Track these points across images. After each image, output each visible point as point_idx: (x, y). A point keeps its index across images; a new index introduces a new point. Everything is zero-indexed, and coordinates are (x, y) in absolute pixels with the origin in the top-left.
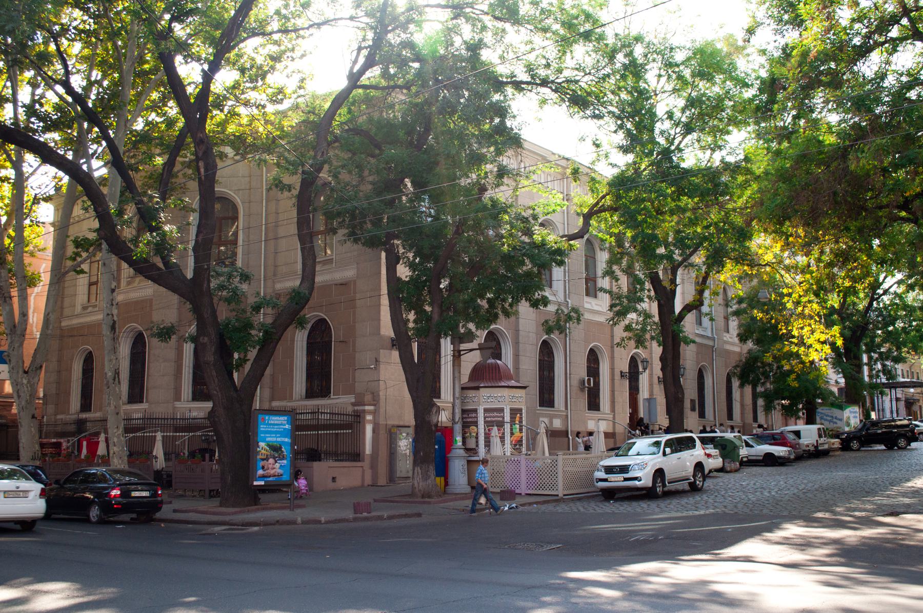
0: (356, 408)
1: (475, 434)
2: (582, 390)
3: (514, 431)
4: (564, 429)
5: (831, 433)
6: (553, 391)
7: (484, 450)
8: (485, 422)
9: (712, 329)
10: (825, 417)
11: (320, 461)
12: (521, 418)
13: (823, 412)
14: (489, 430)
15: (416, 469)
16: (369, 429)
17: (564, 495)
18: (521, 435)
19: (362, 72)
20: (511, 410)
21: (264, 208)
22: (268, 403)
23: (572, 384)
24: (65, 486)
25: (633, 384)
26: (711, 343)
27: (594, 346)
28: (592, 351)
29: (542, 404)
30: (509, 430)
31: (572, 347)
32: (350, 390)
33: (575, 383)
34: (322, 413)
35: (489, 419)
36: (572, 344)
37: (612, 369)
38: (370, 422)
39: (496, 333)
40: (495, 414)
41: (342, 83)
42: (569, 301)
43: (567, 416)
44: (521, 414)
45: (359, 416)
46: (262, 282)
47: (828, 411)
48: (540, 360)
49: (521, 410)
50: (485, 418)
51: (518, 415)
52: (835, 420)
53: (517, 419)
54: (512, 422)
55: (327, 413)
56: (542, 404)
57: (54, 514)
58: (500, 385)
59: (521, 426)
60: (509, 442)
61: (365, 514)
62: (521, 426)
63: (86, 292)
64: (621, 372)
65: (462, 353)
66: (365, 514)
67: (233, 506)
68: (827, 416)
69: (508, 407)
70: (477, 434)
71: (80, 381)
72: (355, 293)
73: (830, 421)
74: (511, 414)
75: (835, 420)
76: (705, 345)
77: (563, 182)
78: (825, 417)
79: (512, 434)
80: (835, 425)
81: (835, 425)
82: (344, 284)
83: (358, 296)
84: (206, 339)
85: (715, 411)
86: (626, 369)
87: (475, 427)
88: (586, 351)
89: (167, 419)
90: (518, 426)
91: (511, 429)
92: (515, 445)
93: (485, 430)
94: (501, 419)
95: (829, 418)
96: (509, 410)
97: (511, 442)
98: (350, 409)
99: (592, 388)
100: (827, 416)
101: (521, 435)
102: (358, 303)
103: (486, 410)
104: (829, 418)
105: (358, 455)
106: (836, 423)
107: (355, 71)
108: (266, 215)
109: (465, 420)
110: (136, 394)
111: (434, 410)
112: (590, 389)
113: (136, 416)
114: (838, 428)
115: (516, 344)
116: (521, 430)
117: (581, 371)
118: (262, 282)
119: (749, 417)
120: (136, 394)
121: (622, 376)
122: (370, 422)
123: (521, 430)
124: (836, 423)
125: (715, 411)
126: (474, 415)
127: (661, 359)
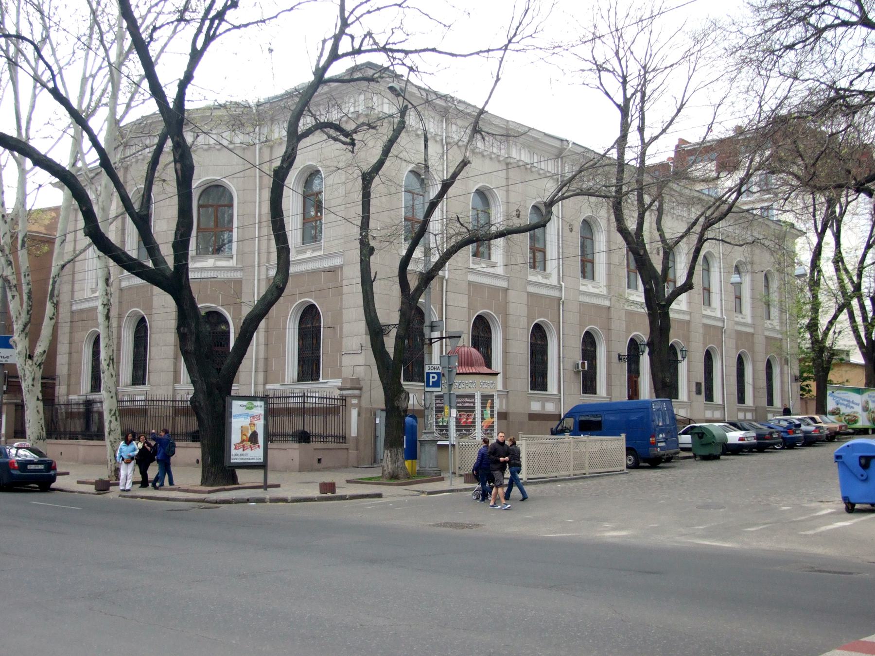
0: (342, 392)
2: (577, 372)
3: (485, 416)
4: (557, 413)
5: (847, 418)
6: (547, 374)
7: (455, 435)
9: (722, 309)
10: (841, 401)
11: (309, 442)
12: (492, 404)
13: (839, 396)
14: (460, 415)
15: (386, 451)
16: (354, 413)
17: (528, 479)
18: (492, 420)
19: (325, 68)
20: (482, 396)
21: (257, 196)
22: (262, 386)
24: (869, 321)
25: (633, 366)
26: (720, 324)
27: (591, 329)
28: (588, 334)
29: (533, 388)
30: (480, 416)
32: (337, 374)
33: (570, 366)
34: (307, 397)
35: (460, 405)
37: (609, 352)
38: (354, 406)
39: (486, 317)
41: (311, 78)
42: (563, 284)
43: (560, 399)
44: (493, 400)
45: (345, 400)
46: (256, 268)
47: (844, 395)
48: (531, 344)
49: (492, 396)
50: (436, 404)
51: (490, 401)
52: (851, 405)
53: (489, 405)
54: (484, 407)
55: (316, 397)
56: (533, 388)
59: (492, 411)
61: (329, 494)
62: (492, 411)
63: (358, 196)
64: (619, 355)
65: (433, 341)
66: (329, 494)
67: (212, 486)
68: (844, 400)
71: (90, 365)
72: (342, 280)
73: (847, 406)
74: (482, 400)
75: (851, 405)
76: (714, 327)
77: (558, 162)
78: (841, 401)
79: (483, 419)
80: (852, 410)
81: (852, 410)
82: (332, 270)
83: (345, 283)
84: (186, 329)
85: (723, 394)
86: (625, 352)
88: (581, 335)
89: (167, 401)
91: (482, 415)
92: (486, 430)
94: (472, 405)
95: (846, 403)
97: (482, 427)
98: (336, 393)
99: (586, 371)
100: (844, 400)
101: (492, 420)
102: (345, 289)
104: (846, 403)
105: (344, 437)
106: (853, 408)
107: (320, 66)
108: (259, 202)
109: (437, 405)
110: (139, 376)
111: (403, 396)
112: (584, 373)
113: (138, 398)
114: (854, 413)
115: (505, 328)
117: (576, 355)
118: (256, 268)
119: (764, 401)
120: (139, 376)
121: (620, 359)
122: (354, 406)
123: (492, 416)
124: (853, 408)
125: (723, 394)
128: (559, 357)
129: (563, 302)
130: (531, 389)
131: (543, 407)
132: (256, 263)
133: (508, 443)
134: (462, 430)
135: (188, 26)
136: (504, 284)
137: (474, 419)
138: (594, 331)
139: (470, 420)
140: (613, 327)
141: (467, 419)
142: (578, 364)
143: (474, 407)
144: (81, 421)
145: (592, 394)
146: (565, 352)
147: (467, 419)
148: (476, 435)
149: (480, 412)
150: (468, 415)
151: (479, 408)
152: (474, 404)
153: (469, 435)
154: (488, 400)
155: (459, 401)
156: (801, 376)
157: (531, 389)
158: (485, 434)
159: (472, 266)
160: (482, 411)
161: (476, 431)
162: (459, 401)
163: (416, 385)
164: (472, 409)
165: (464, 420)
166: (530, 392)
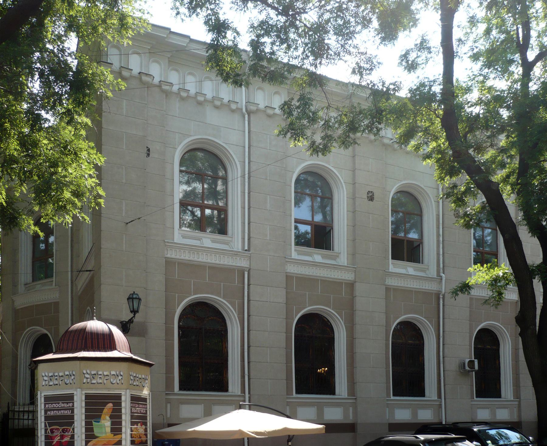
8: (47, 418)
35: (52, 413)
46: (70, 273)
50: (46, 412)
51: (110, 405)
93: (46, 430)
101: (117, 438)
103: (48, 399)
116: (116, 429)
129: (444, 296)
130: (394, 395)
131: (415, 414)
132: (69, 269)
136: (348, 276)
137: (73, 437)
138: (495, 328)
139: (66, 439)
141: (62, 437)
142: (464, 364)
143: (72, 417)
144: (490, 418)
145: (330, 394)
146: (446, 350)
147: (62, 437)
150: (63, 431)
152: (73, 411)
154: (105, 404)
157: (394, 395)
159: (294, 255)
164: (69, 420)
165: (57, 439)
166: (392, 398)
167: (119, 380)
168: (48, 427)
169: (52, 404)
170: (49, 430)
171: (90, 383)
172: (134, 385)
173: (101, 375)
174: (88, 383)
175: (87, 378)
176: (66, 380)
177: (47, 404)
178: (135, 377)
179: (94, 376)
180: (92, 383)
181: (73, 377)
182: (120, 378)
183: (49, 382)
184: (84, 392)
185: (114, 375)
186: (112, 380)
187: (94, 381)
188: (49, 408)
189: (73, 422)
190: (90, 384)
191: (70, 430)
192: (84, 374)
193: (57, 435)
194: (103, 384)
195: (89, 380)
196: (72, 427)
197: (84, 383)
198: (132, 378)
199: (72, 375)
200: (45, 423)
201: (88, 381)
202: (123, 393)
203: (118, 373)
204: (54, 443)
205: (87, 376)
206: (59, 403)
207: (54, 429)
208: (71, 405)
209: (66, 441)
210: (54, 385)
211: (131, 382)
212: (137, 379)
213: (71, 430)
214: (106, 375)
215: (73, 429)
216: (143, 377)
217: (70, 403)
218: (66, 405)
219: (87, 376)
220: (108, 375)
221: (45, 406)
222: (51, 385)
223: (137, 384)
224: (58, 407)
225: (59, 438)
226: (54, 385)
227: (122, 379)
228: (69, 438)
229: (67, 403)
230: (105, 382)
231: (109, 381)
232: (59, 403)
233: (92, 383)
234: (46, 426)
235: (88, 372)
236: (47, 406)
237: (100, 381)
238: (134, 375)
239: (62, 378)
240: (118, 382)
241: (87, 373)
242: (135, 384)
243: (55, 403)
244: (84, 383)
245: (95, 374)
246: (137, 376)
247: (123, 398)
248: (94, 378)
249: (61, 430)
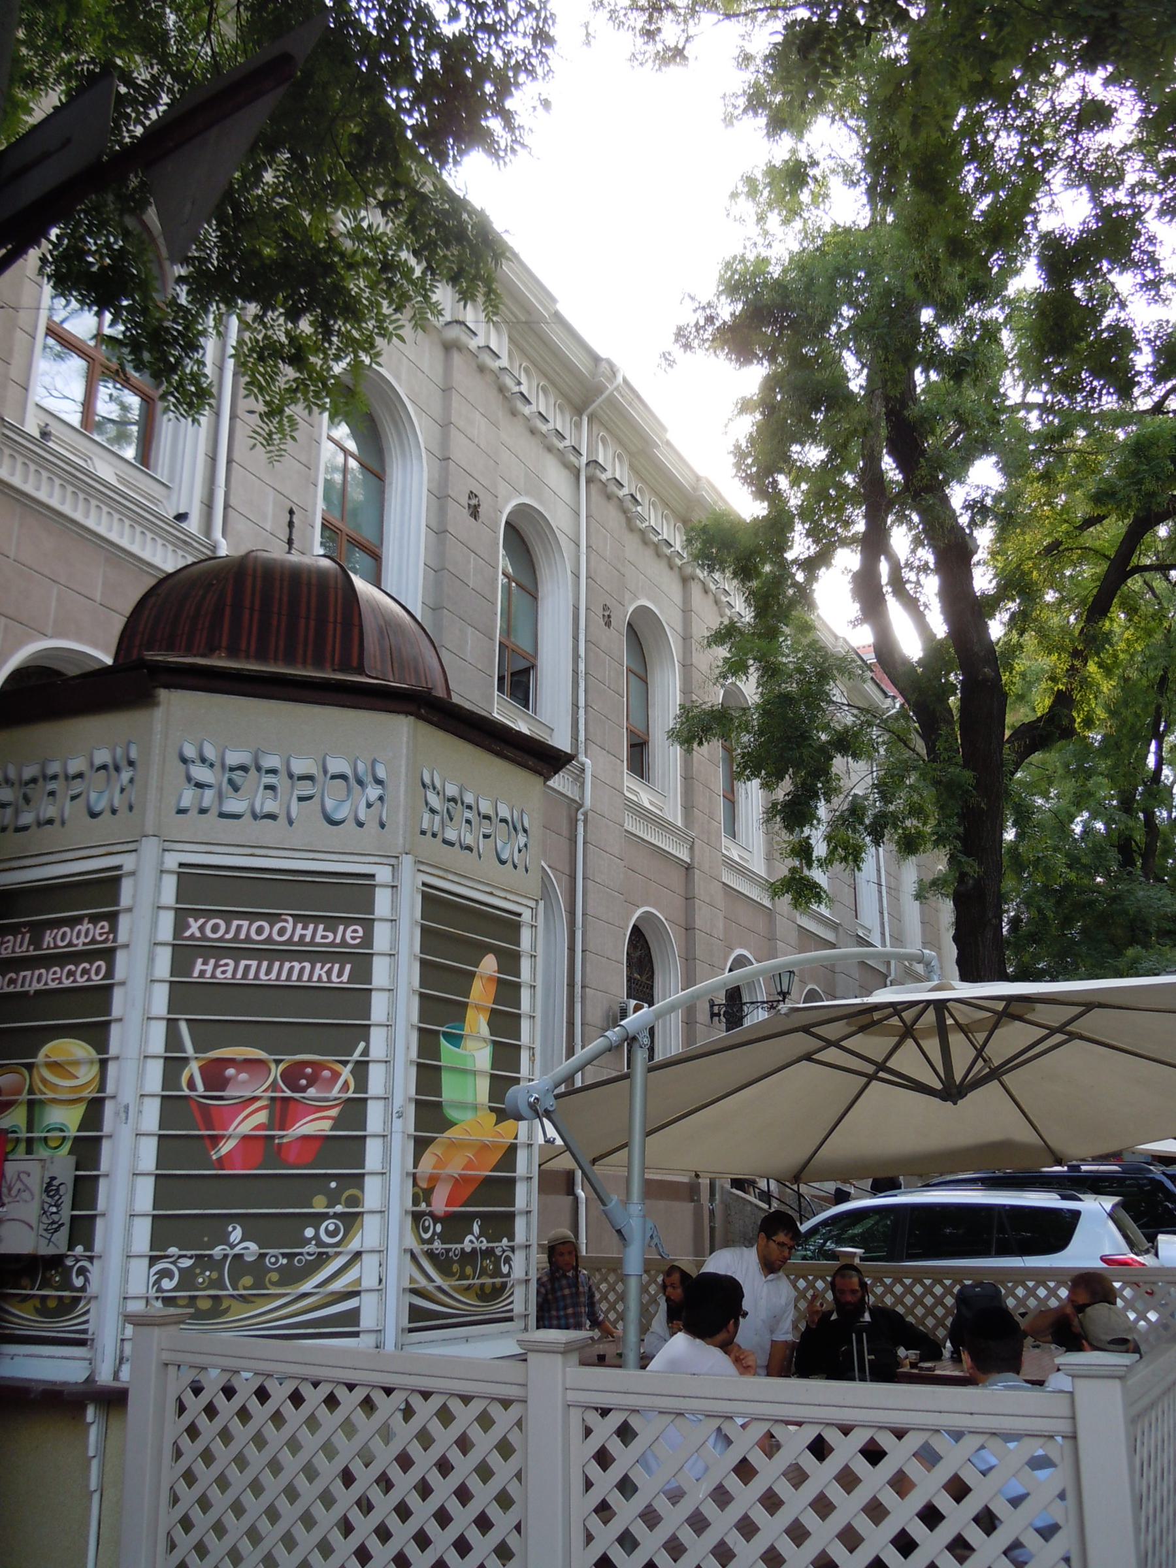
1: (68, 1118)
7: (140, 1277)
12: (508, 991)
14: (215, 1076)
23: (590, 1018)
27: (648, 916)
30: (405, 1085)
31: (590, 903)
35: (227, 971)
36: (591, 896)
40: (290, 930)
43: (628, 1180)
44: (510, 961)
51: (489, 965)
53: (481, 993)
57: (528, 1224)
58: (405, 614)
60: (400, 1198)
69: (411, 881)
70: (94, 1109)
87: (77, 1049)
88: (624, 928)
90: (480, 1056)
92: (455, 1225)
93: (173, 1065)
94: (339, 976)
96: (411, 909)
97: (423, 1194)
126: (81, 936)
127: (956, 939)
128: (571, 985)
133: (934, 838)
134: (217, 1229)
135: (726, 21)
140: (698, 923)
148: (367, 1272)
149: (407, 1047)
150: (291, 1077)
151: (409, 1011)
152: (362, 962)
153: (293, 1275)
155: (218, 930)
156: (1080, 767)
158: (442, 1263)
160: (428, 1042)
161: (368, 1235)
162: (218, 930)
163: (421, 499)
167: (369, 806)
168: (190, 1050)
169: (228, 916)
170: (194, 1068)
171: (214, 812)
172: (446, 842)
173: (273, 771)
174: (203, 811)
175: (200, 785)
176: (93, 796)
177: (197, 914)
178: (453, 800)
179: (237, 776)
180: (222, 815)
181: (126, 775)
182: (373, 792)
183: (220, 796)
184: (172, 861)
185: (343, 777)
186: (329, 804)
187: (234, 805)
188: (204, 938)
189: (363, 1032)
190: (212, 816)
191: (336, 1075)
192: (184, 761)
193: (255, 1099)
194: (282, 820)
195: (209, 794)
196: (356, 1056)
197: (181, 811)
198: (434, 801)
199: (123, 763)
200: (172, 1024)
201: (206, 804)
202: (383, 874)
203: (361, 767)
204: (226, 1147)
205: (201, 773)
206: (276, 918)
207: (231, 1062)
208: (352, 934)
209: (306, 1138)
210: (255, 816)
211: (426, 821)
212: (468, 814)
213: (346, 1073)
214: (301, 778)
215: (361, 1069)
216: (504, 812)
217: (348, 921)
218: (320, 935)
219: (201, 773)
220: (310, 778)
221: (180, 926)
222: (237, 816)
223: (469, 840)
224: (269, 940)
225: (262, 1117)
226: (255, 816)
227: (381, 798)
228: (327, 1124)
229: (331, 924)
230: (294, 815)
231: (314, 804)
232: (273, 918)
233: (222, 815)
234: (173, 1040)
235: (210, 753)
236: (194, 927)
237: (270, 806)
238: (451, 790)
239: (305, 789)
240: (362, 817)
241: (203, 760)
242: (451, 835)
243: (252, 917)
244: (181, 811)
245: (244, 768)
246: (469, 798)
247: (382, 902)
248: (236, 789)
249: (276, 1072)
